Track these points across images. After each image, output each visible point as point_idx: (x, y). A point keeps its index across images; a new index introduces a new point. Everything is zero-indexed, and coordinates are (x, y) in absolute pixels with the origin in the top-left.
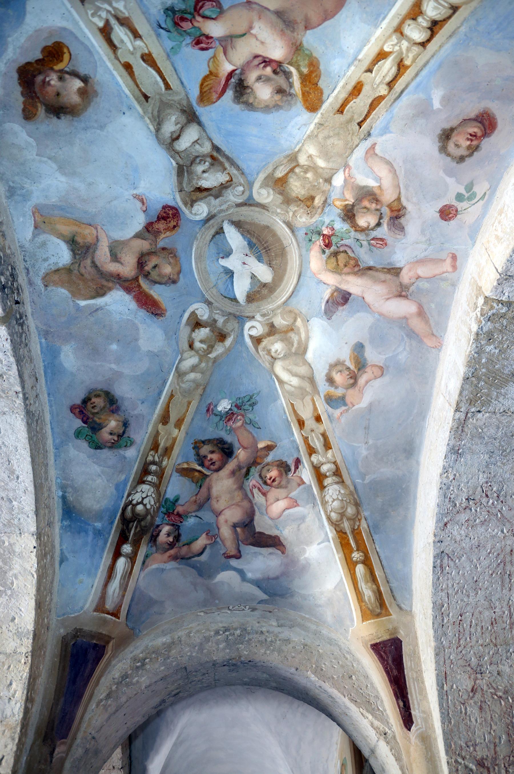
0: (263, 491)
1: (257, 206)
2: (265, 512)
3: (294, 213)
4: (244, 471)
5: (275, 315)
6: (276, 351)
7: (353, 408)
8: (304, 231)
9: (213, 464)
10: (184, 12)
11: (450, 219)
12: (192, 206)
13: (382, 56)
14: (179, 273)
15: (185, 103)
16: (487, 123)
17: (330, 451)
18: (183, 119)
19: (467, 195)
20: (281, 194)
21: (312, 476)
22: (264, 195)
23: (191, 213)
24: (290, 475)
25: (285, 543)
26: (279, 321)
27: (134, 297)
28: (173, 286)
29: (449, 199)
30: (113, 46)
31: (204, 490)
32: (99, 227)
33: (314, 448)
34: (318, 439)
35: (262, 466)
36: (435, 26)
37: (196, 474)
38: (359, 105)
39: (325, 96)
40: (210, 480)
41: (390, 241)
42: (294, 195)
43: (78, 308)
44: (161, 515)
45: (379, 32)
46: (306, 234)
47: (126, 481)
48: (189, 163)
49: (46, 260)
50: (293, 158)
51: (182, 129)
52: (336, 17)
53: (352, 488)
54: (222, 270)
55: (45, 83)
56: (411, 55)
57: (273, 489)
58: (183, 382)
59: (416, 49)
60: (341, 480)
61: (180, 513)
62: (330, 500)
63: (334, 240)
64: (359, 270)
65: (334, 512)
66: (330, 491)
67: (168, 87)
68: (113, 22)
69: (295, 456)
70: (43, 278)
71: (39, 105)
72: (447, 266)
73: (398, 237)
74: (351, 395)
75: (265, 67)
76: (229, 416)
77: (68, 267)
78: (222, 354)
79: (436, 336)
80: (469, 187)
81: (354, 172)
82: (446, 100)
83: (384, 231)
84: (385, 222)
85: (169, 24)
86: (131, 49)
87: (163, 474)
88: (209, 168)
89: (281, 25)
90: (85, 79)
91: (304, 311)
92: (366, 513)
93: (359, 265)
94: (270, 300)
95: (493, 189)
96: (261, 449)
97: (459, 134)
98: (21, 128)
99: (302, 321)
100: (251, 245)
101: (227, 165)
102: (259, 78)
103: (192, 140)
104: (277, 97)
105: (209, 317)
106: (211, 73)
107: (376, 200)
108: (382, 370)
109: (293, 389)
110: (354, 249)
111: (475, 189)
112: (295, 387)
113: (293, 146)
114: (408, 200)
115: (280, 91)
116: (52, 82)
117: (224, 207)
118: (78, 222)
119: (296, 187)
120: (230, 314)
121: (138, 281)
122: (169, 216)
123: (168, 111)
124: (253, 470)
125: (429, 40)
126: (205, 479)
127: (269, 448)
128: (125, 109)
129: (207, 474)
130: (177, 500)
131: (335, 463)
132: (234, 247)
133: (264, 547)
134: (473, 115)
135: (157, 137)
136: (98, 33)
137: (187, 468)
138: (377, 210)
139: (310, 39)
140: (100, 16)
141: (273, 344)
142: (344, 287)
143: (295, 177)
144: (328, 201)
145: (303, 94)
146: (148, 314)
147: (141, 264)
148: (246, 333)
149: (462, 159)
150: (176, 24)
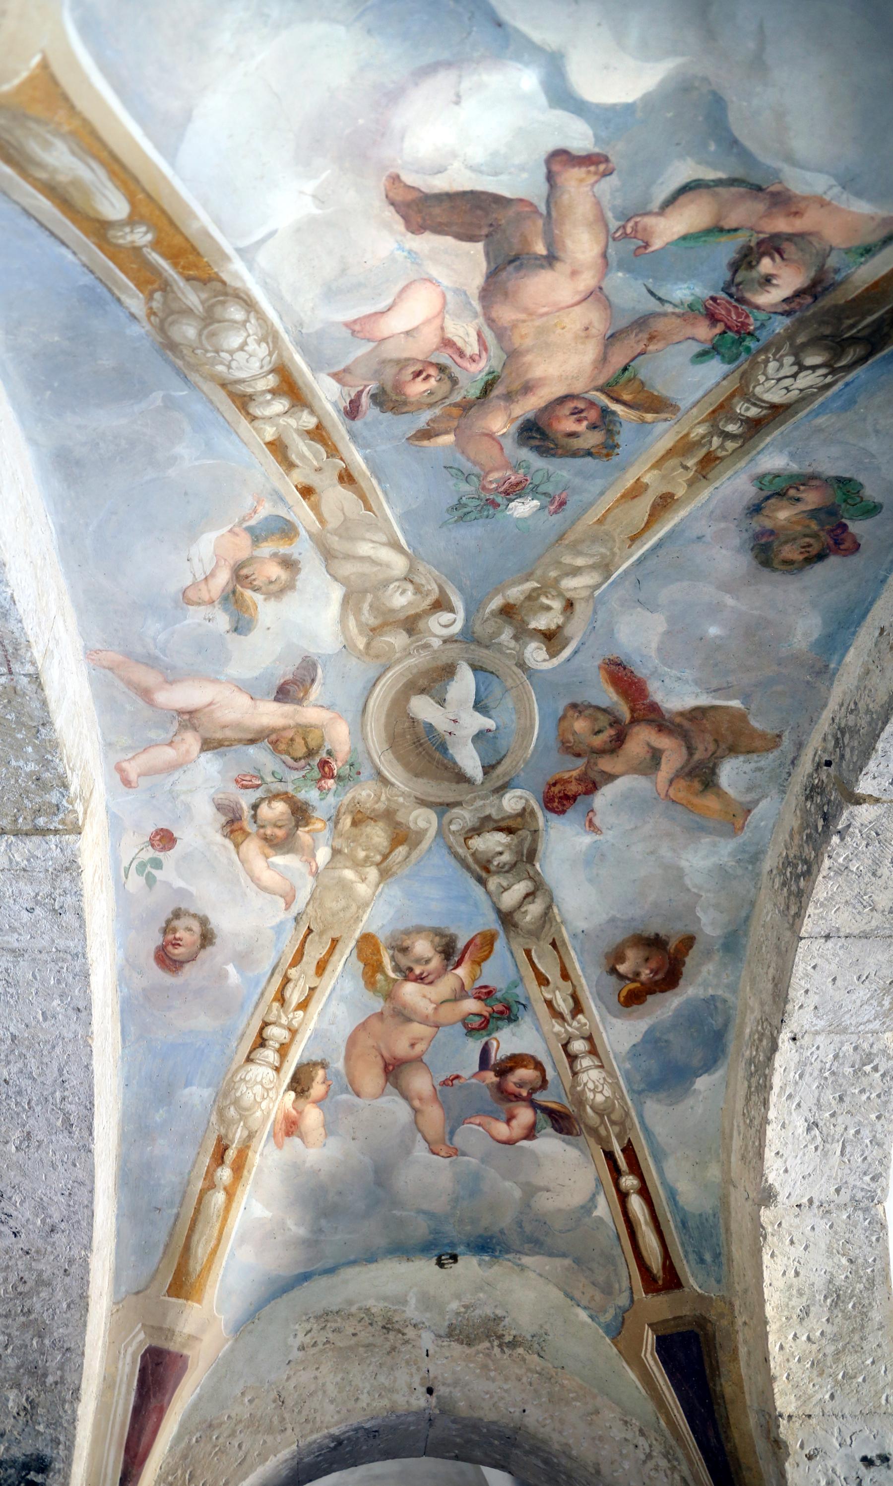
0: (450, 351)
1: (432, 803)
2: (450, 296)
3: (378, 800)
4: (498, 390)
5: (405, 649)
6: (403, 592)
7: (229, 527)
8: (362, 777)
9: (576, 412)
10: (498, 1019)
11: (157, 833)
12: (524, 809)
13: (303, 1005)
14: (563, 718)
15: (512, 934)
16: (167, 962)
17: (269, 438)
18: (517, 917)
19: (148, 868)
20: (399, 824)
21: (312, 390)
22: (423, 819)
23: (527, 800)
24: (372, 386)
25: (390, 213)
26: (398, 640)
27: (646, 697)
28: (578, 700)
29: (169, 858)
30: (575, 997)
31: (618, 360)
32: (663, 796)
33: (312, 439)
34: (303, 457)
35: (448, 402)
36: (262, 1042)
37: (626, 397)
38: (315, 952)
39: (355, 953)
40: (594, 379)
41: (233, 788)
42: (381, 824)
43: (746, 697)
44: (764, 335)
45: (312, 1026)
46: (359, 773)
47: (817, 413)
48: (519, 865)
49: (760, 769)
50: (385, 874)
51: (520, 905)
52: (354, 1028)
53: (194, 377)
54: (493, 713)
55: (655, 972)
56: (275, 1012)
57: (421, 357)
58: (603, 556)
59: (272, 1018)
60: (230, 387)
61: (707, 322)
62: (252, 346)
63: (316, 774)
64: (268, 736)
65: (235, 322)
66: (258, 364)
67: (528, 953)
68: (568, 1017)
69: (358, 424)
70: (777, 746)
71: (672, 951)
72: (132, 769)
73: (222, 796)
74: (242, 547)
75: (422, 974)
76: (514, 491)
77: (732, 754)
78: (514, 584)
79: (104, 667)
80: (151, 881)
81: (305, 870)
82: (222, 976)
83: (245, 800)
84: (247, 813)
85: (515, 1008)
86: (557, 993)
87: (714, 412)
88: (493, 857)
89: (406, 1012)
90: (613, 971)
91: (354, 661)
92: (140, 331)
93: (271, 743)
94: (415, 671)
95: (120, 887)
96: (446, 432)
97: (194, 943)
98: (704, 928)
99: (355, 646)
100: (443, 747)
101: (470, 860)
102: (428, 961)
103: (510, 891)
104: (407, 943)
105: (525, 645)
106: (479, 964)
107: (266, 839)
108: (187, 598)
109: (368, 535)
110: (283, 766)
111: (142, 880)
112: (364, 539)
113: (386, 890)
114: (224, 846)
115: (404, 950)
116: (648, 972)
117: (479, 803)
118: (689, 807)
119: (378, 835)
120: (487, 647)
121: (632, 717)
122: (559, 799)
123: (532, 927)
124: (474, 391)
125: (262, 1029)
126: (608, 384)
127: (427, 434)
128: (581, 936)
129: (598, 394)
130: (702, 356)
131: (253, 419)
132: (470, 745)
133: (464, 194)
134: (187, 967)
135: (552, 899)
136: (585, 1010)
137: (647, 411)
138: (263, 827)
139: (378, 1004)
140: (579, 1022)
141: (410, 604)
142: (288, 708)
143: (381, 848)
144: (332, 825)
145: (379, 951)
146: (632, 668)
147: (620, 739)
148: (461, 615)
149: (177, 914)
150: (508, 1008)
